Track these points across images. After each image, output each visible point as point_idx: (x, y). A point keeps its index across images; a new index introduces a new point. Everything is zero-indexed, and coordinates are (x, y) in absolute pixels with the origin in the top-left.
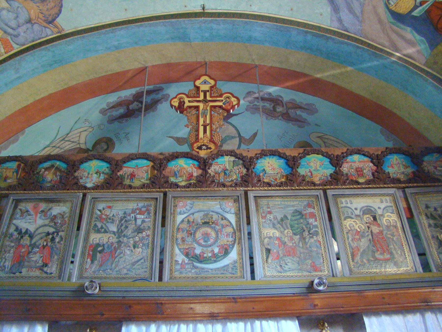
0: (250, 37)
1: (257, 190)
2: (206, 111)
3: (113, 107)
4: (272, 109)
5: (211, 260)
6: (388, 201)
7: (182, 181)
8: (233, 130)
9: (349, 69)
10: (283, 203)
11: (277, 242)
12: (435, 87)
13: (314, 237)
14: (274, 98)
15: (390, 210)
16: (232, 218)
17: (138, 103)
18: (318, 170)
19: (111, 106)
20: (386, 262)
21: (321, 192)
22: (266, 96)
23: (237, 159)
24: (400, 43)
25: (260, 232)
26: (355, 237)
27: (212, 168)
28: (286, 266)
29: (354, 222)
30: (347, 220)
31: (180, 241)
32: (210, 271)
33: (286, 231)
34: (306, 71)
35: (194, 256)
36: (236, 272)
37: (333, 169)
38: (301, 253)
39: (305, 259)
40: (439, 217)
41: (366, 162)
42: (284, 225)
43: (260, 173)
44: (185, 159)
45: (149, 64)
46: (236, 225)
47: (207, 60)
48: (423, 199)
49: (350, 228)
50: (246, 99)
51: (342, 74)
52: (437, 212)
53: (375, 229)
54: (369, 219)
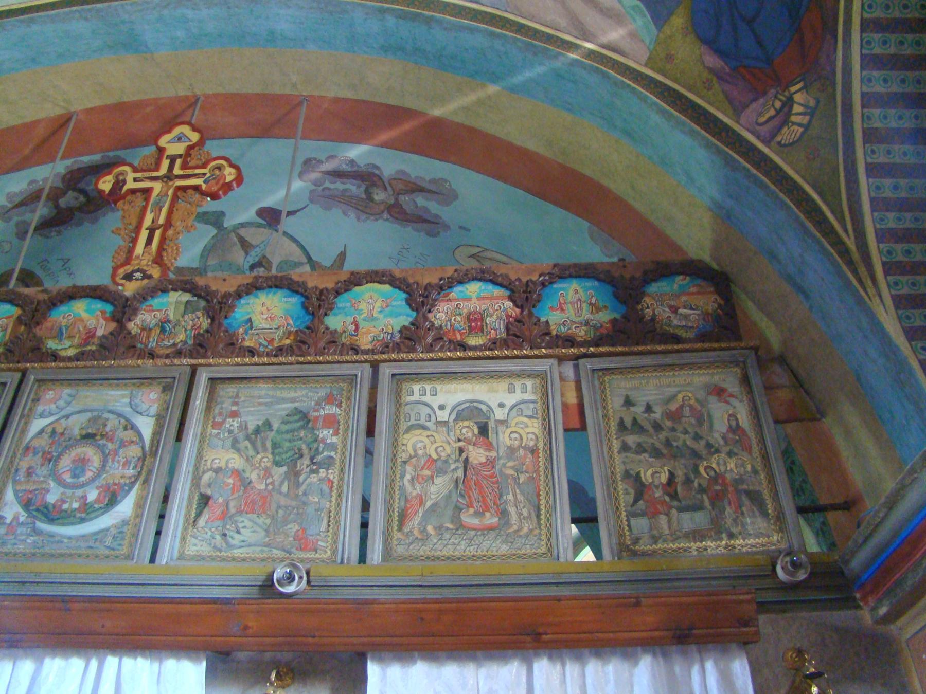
0: (272, 33)
1: (219, 365)
2: (165, 198)
3: (22, 204)
4: (364, 196)
5: (74, 516)
6: (529, 388)
7: (70, 347)
8: (298, 251)
9: (492, 89)
10: (271, 393)
11: (231, 481)
12: (663, 112)
13: (321, 470)
14: (361, 172)
15: (528, 410)
16: (146, 427)
17: (75, 194)
18: (376, 319)
19: (17, 200)
20: (484, 534)
21: (367, 367)
22: (344, 166)
23: (196, 298)
24: (591, 18)
25: (200, 457)
26: (420, 473)
27: (138, 320)
28: (236, 536)
29: (428, 436)
30: (413, 432)
31: (21, 476)
32: (66, 541)
33: (259, 456)
34: (410, 103)
35: (41, 508)
36: (120, 545)
37: (411, 316)
38: (279, 507)
39: (286, 522)
40: (653, 427)
41: (497, 298)
42: (259, 443)
43: (239, 327)
44: (88, 300)
45: (76, 107)
46: (152, 440)
47: (198, 92)
48: (623, 384)
49: (415, 451)
50: (305, 177)
51: (480, 102)
52: (653, 415)
53: (477, 455)
54: (467, 432)
